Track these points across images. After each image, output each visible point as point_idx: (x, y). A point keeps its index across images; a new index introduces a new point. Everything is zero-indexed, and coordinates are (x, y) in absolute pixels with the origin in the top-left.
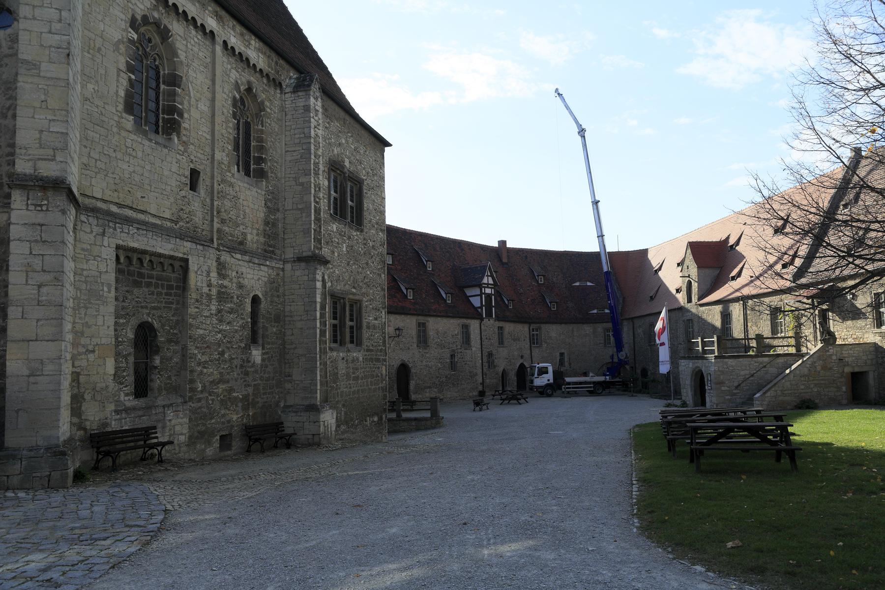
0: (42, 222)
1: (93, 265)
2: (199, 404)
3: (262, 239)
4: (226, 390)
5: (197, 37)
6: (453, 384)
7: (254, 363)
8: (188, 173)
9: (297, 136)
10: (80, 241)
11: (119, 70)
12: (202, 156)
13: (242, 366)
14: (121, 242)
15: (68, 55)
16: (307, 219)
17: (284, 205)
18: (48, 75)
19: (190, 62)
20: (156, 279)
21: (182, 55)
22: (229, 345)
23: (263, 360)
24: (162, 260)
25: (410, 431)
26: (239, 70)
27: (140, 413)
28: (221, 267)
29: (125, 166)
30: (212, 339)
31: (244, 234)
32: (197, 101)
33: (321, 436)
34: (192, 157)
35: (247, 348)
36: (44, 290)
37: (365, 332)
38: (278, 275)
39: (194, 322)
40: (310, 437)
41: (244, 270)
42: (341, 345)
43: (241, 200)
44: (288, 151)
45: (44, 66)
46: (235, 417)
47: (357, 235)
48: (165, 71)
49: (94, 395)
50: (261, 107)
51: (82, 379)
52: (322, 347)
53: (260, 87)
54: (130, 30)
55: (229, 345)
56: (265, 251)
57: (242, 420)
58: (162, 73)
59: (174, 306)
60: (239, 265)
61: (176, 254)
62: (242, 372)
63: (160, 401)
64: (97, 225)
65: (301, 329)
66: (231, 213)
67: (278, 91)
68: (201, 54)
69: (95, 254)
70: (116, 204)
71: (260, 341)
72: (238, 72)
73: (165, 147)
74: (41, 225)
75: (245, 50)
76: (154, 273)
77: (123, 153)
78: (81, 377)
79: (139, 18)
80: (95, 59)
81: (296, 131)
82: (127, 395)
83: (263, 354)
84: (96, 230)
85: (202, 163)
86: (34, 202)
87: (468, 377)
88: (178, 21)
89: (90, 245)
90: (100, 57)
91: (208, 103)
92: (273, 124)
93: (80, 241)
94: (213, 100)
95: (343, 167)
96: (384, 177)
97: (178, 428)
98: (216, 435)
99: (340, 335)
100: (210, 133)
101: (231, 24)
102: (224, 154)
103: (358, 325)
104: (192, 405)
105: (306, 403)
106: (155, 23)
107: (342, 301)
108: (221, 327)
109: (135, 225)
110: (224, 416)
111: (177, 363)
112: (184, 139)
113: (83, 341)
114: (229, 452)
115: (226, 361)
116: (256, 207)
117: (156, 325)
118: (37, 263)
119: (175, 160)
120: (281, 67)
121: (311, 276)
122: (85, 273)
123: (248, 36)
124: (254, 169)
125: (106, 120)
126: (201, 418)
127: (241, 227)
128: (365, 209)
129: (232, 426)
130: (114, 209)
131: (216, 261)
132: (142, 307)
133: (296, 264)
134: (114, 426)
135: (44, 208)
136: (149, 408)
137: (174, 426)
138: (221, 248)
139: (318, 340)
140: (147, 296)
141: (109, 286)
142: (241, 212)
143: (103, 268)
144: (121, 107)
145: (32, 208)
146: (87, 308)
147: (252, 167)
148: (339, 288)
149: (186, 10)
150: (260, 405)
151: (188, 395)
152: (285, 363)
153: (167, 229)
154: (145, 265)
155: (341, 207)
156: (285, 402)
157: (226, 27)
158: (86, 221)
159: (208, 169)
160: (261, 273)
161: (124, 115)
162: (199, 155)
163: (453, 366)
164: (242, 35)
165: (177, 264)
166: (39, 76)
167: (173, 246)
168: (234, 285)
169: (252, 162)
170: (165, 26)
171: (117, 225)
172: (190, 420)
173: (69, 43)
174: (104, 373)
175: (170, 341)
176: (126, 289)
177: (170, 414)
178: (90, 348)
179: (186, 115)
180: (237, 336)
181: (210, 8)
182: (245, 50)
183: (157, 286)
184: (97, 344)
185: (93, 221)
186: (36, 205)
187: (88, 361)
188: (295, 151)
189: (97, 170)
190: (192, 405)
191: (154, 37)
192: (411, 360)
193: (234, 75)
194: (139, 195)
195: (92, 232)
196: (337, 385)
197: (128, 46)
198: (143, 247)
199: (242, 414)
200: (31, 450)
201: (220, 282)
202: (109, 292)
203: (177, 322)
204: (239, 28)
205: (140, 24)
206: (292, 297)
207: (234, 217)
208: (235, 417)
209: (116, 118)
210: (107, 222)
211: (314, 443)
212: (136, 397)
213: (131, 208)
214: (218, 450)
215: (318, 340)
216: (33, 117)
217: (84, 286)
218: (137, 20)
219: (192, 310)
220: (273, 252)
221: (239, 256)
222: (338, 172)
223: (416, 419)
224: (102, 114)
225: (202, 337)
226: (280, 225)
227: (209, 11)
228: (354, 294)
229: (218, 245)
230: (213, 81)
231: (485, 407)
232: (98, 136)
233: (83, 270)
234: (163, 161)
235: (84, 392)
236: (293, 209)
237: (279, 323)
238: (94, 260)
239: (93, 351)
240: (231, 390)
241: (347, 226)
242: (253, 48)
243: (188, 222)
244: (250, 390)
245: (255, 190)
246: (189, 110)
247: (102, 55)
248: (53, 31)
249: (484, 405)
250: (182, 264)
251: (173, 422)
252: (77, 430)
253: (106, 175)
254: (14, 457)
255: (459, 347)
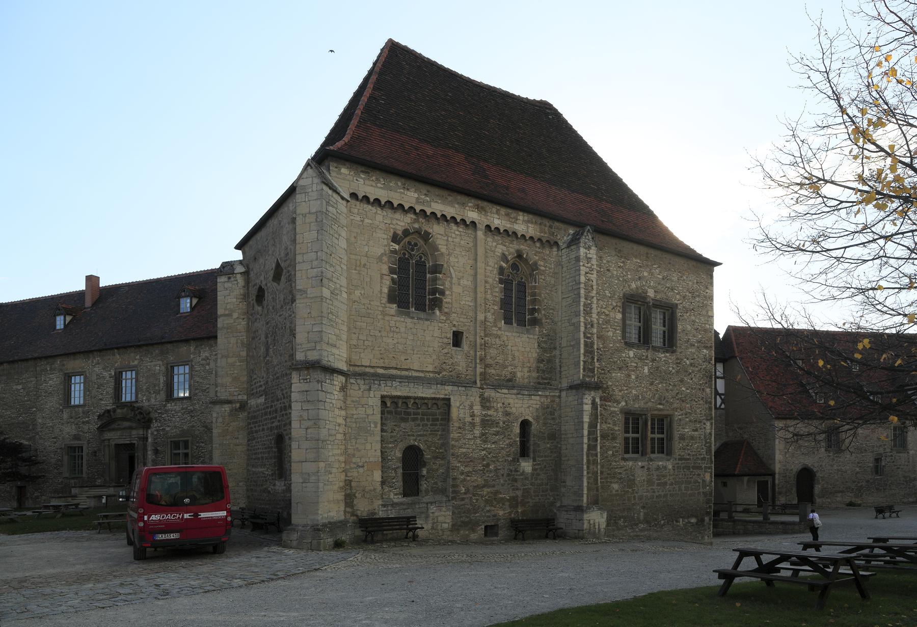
0: (307, 389)
1: (361, 411)
2: (463, 502)
3: (535, 375)
4: (492, 493)
5: (458, 231)
6: (877, 489)
7: (524, 472)
8: (450, 335)
9: (571, 284)
10: (350, 396)
11: (382, 275)
12: (465, 320)
13: (508, 475)
14: (385, 393)
15: (322, 280)
16: (577, 353)
17: (561, 344)
18: (311, 296)
19: (451, 251)
20: (422, 415)
21: (443, 249)
22: (494, 459)
23: (534, 469)
24: (426, 401)
25: (776, 533)
26: (507, 244)
27: (405, 507)
28: (485, 402)
29: (390, 340)
30: (476, 456)
31: (514, 374)
32: (459, 279)
33: (585, 531)
34: (455, 323)
35: (515, 460)
36: (309, 431)
37: (677, 443)
38: (553, 401)
39: (457, 444)
40: (577, 532)
41: (511, 401)
42: (642, 455)
43: (509, 347)
44: (564, 298)
45: (309, 291)
46: (501, 513)
47: (665, 357)
48: (430, 264)
49: (364, 494)
50: (535, 267)
51: (353, 484)
52: (591, 458)
53: (532, 253)
54: (392, 243)
55: (494, 459)
56: (539, 383)
57: (510, 515)
58: (427, 265)
59: (440, 433)
60: (506, 398)
61: (438, 396)
62: (509, 479)
63: (426, 499)
64: (364, 384)
65: (572, 444)
66: (498, 358)
67: (555, 249)
68: (462, 242)
69: (363, 403)
70: (382, 367)
71: (532, 455)
72: (505, 246)
73: (427, 320)
74: (307, 391)
75: (512, 226)
76: (420, 411)
77: (388, 332)
78: (352, 483)
79: (400, 233)
80: (361, 272)
81: (570, 280)
82: (396, 494)
83: (534, 465)
84: (363, 387)
85: (466, 325)
86: (303, 377)
87: (902, 482)
88: (439, 223)
89: (359, 398)
90: (366, 270)
91: (471, 279)
92: (548, 279)
93: (350, 396)
94: (475, 275)
95: (645, 297)
96: (713, 296)
97: (441, 519)
98: (481, 525)
99: (642, 446)
100: (473, 301)
101: (494, 210)
102: (491, 312)
103: (669, 437)
104: (455, 503)
105: (575, 504)
106: (417, 232)
107: (644, 417)
108: (486, 446)
109: (397, 380)
110: (489, 511)
111: (443, 473)
112: (446, 310)
113: (354, 460)
114: (495, 538)
115: (491, 471)
116: (528, 349)
117: (422, 446)
118: (305, 415)
119: (436, 328)
120: (557, 228)
121: (580, 401)
122: (355, 416)
123: (513, 214)
124: (528, 319)
125: (372, 312)
126: (464, 512)
127: (509, 368)
128: (679, 331)
129: (499, 520)
130: (380, 371)
131: (480, 397)
132: (409, 435)
133: (569, 391)
134: (381, 514)
135: (308, 381)
136: (414, 503)
137: (437, 517)
138: (485, 387)
139: (585, 453)
140: (414, 427)
141: (375, 424)
142: (509, 356)
143: (370, 411)
144: (385, 300)
145: (302, 381)
146: (357, 439)
147: (527, 317)
148: (637, 406)
149: (444, 213)
150: (531, 505)
151: (451, 495)
152: (561, 472)
153: (430, 379)
154: (410, 406)
155: (644, 334)
156: (561, 503)
157: (489, 214)
158: (354, 382)
159: (472, 329)
160: (532, 402)
161: (388, 305)
162: (461, 320)
163: (878, 469)
164: (507, 215)
165: (440, 403)
166: (307, 298)
167: (434, 391)
168: (500, 413)
169: (527, 313)
170: (426, 232)
171: (381, 382)
172: (453, 513)
173: (322, 272)
174: (373, 480)
175: (436, 458)
176: (394, 424)
177: (433, 508)
178: (360, 464)
179: (447, 293)
180: (504, 452)
181: (470, 204)
182: (512, 226)
183: (422, 420)
184: (366, 462)
185: (361, 382)
186: (304, 379)
187: (358, 472)
188: (568, 297)
189: (365, 347)
190: (455, 503)
191: (419, 241)
192: (816, 465)
193: (500, 249)
194: (403, 358)
195: (360, 389)
196: (633, 490)
197: (390, 256)
198: (405, 395)
199: (509, 510)
200: (303, 527)
201: (484, 413)
202: (376, 427)
203: (443, 445)
204: (503, 211)
205: (401, 237)
206: (567, 418)
207: (501, 361)
208: (501, 513)
209: (381, 309)
210: (372, 381)
211: (579, 537)
212: (405, 495)
213: (396, 368)
214: (483, 536)
215: (585, 453)
216: (304, 325)
217: (354, 425)
218: (398, 235)
219: (454, 435)
220: (548, 383)
221: (505, 391)
222: (640, 303)
223: (782, 523)
224: (368, 308)
225: (465, 454)
226: (557, 361)
227: (469, 207)
228: (660, 410)
229: (481, 384)
230: (476, 260)
231: (894, 515)
232: (365, 324)
233: (353, 414)
234: (425, 330)
235: (356, 493)
236: (567, 346)
237: (555, 440)
238: (363, 407)
239: (363, 466)
240: (497, 492)
241: (650, 351)
242: (521, 222)
243: (451, 372)
244: (519, 493)
245: (526, 336)
246: (451, 288)
247: (367, 269)
248: (313, 267)
249: (894, 512)
250: (446, 402)
251: (436, 514)
252: (351, 516)
253: (373, 349)
254: (294, 530)
255: (888, 450)
